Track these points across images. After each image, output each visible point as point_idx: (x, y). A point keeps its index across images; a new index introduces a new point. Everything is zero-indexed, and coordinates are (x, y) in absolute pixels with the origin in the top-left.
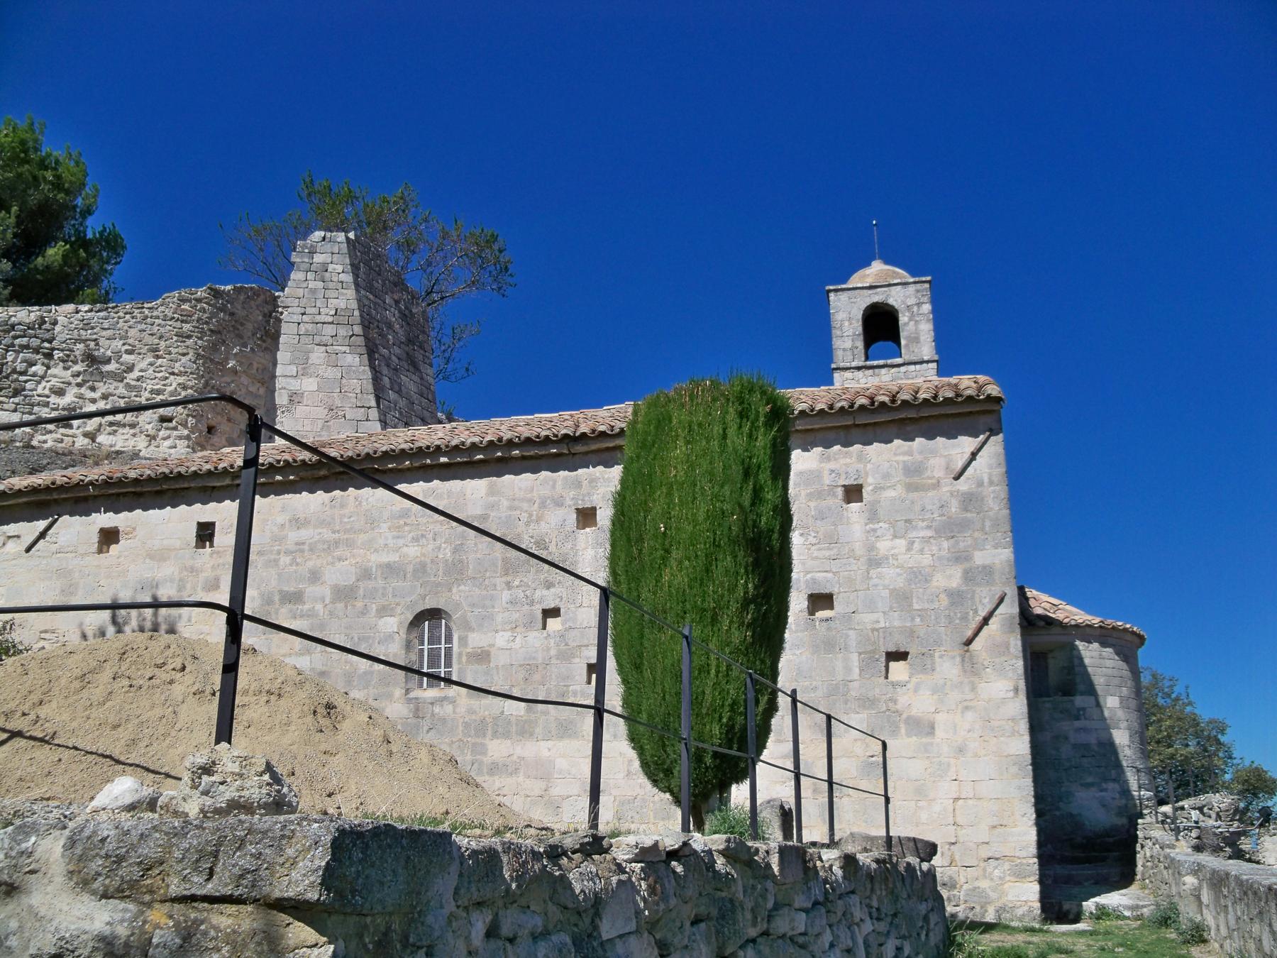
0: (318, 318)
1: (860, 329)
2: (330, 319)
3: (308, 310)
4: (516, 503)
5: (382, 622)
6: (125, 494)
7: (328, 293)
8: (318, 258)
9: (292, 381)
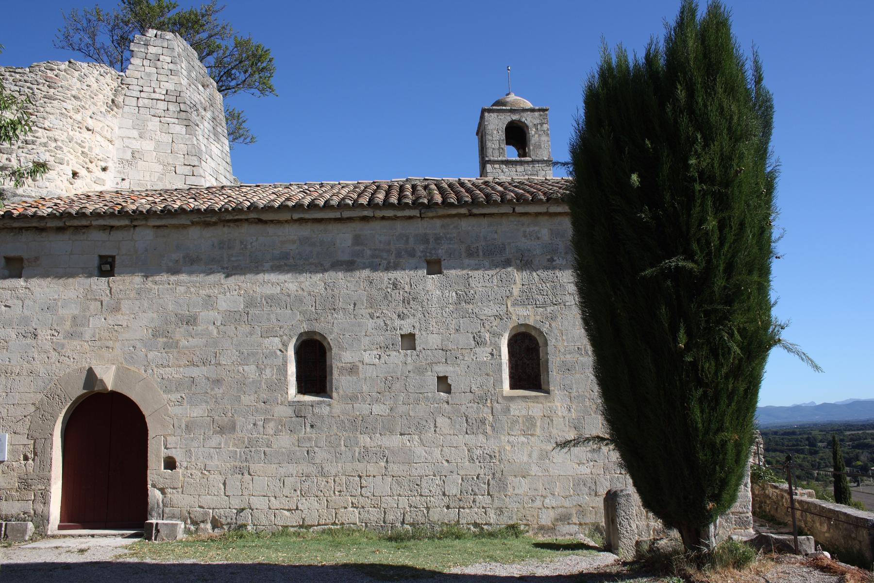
0: (154, 96)
1: (504, 137)
2: (163, 98)
3: (145, 89)
4: (377, 252)
5: (266, 341)
6: (27, 229)
7: (161, 77)
8: (152, 50)
9: (134, 141)
